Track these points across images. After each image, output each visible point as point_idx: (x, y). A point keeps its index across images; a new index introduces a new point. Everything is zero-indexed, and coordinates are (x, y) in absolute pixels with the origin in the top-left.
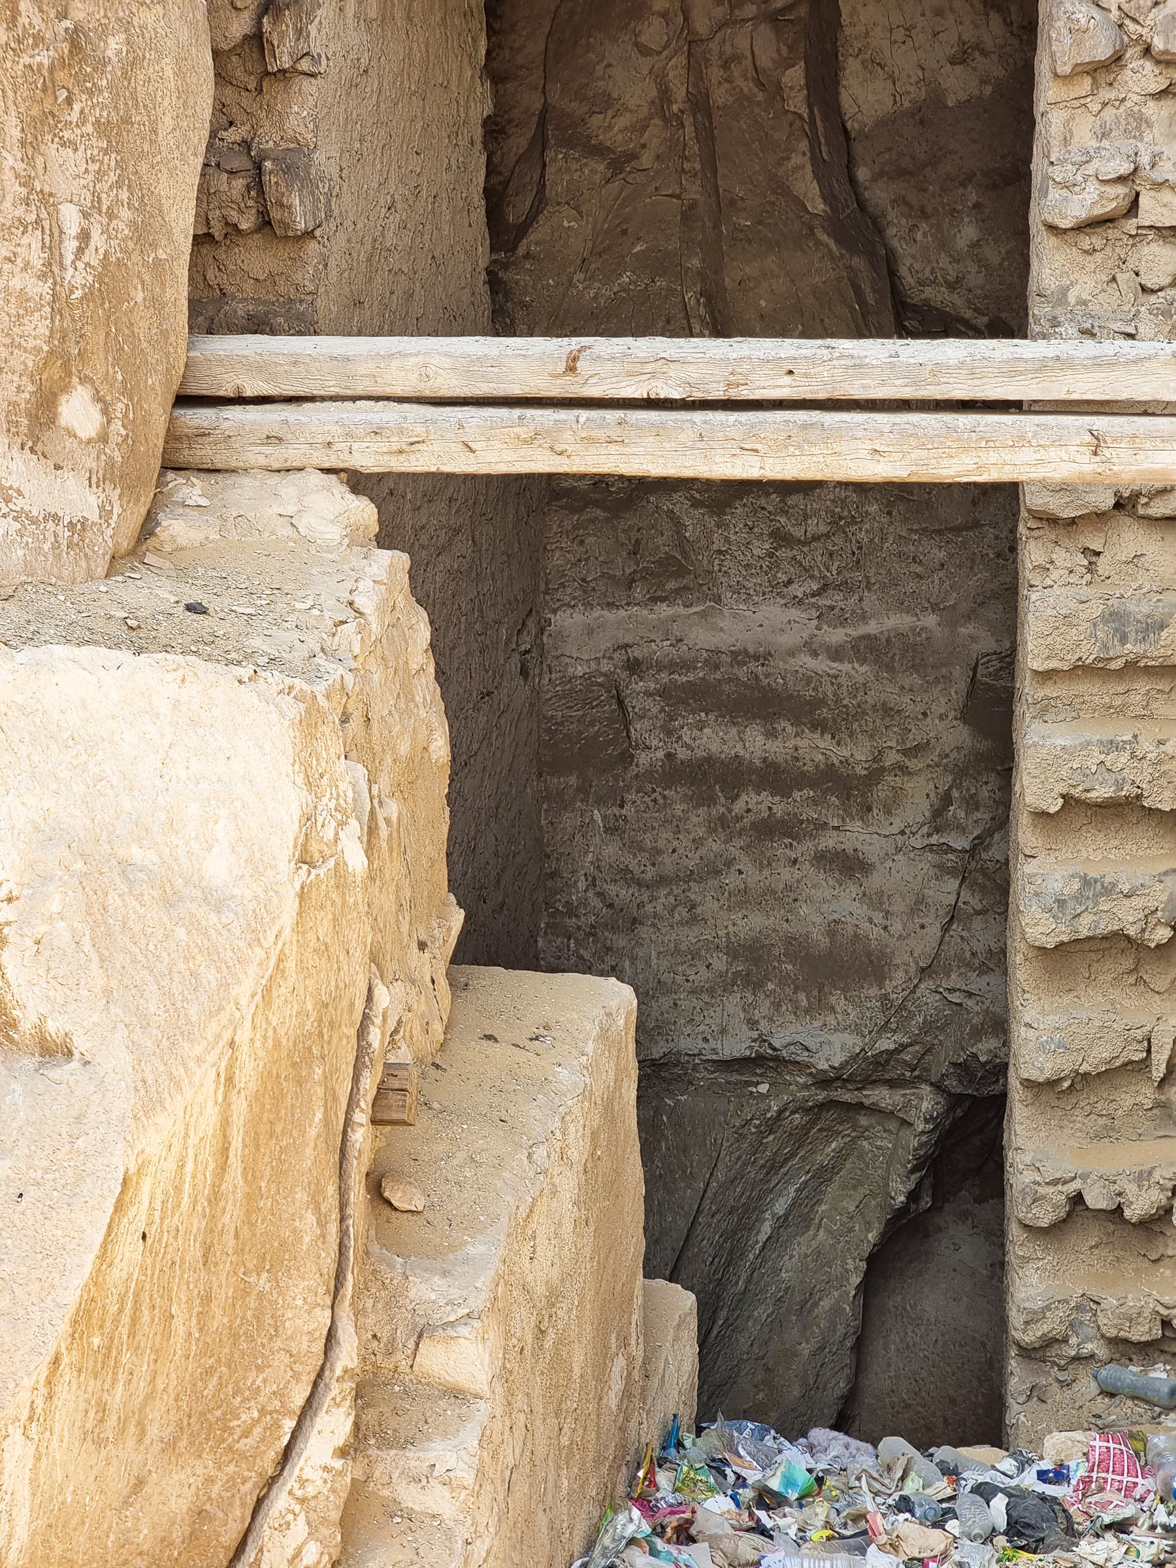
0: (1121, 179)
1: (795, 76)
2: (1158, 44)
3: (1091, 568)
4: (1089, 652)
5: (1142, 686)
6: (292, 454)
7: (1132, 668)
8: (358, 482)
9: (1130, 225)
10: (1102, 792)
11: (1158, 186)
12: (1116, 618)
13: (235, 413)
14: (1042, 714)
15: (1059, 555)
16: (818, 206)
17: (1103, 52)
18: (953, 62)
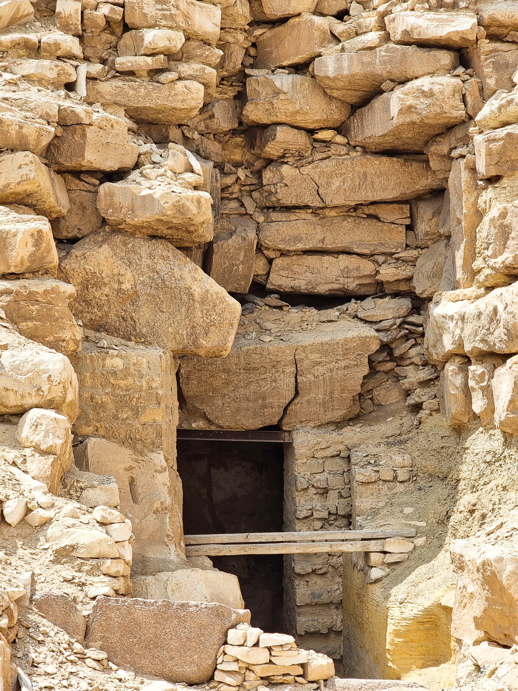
0: (310, 509)
1: (204, 491)
2: (315, 485)
3: (307, 585)
4: (308, 601)
5: (318, 608)
6: (200, 553)
7: (317, 604)
8: (210, 557)
9: (312, 518)
10: (312, 630)
11: (316, 510)
12: (313, 594)
13: (201, 547)
14: (299, 616)
15: (301, 582)
16: (211, 521)
17: (306, 487)
18: (239, 487)
